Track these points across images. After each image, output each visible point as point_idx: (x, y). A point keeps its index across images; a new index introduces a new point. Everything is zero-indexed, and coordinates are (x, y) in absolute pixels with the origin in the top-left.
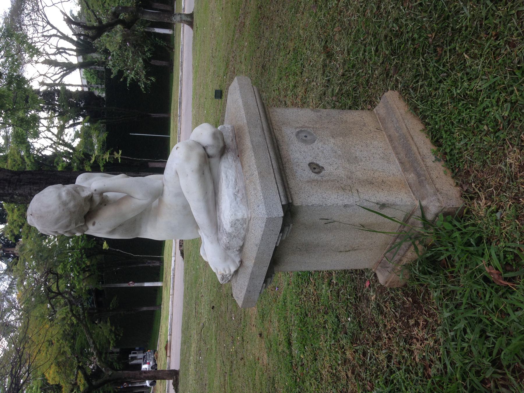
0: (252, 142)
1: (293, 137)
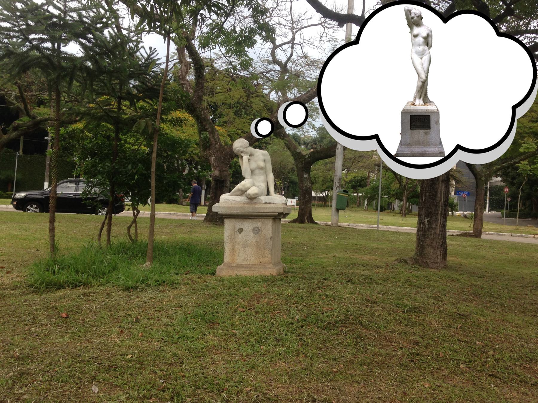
0: (245, 207)
1: (256, 226)
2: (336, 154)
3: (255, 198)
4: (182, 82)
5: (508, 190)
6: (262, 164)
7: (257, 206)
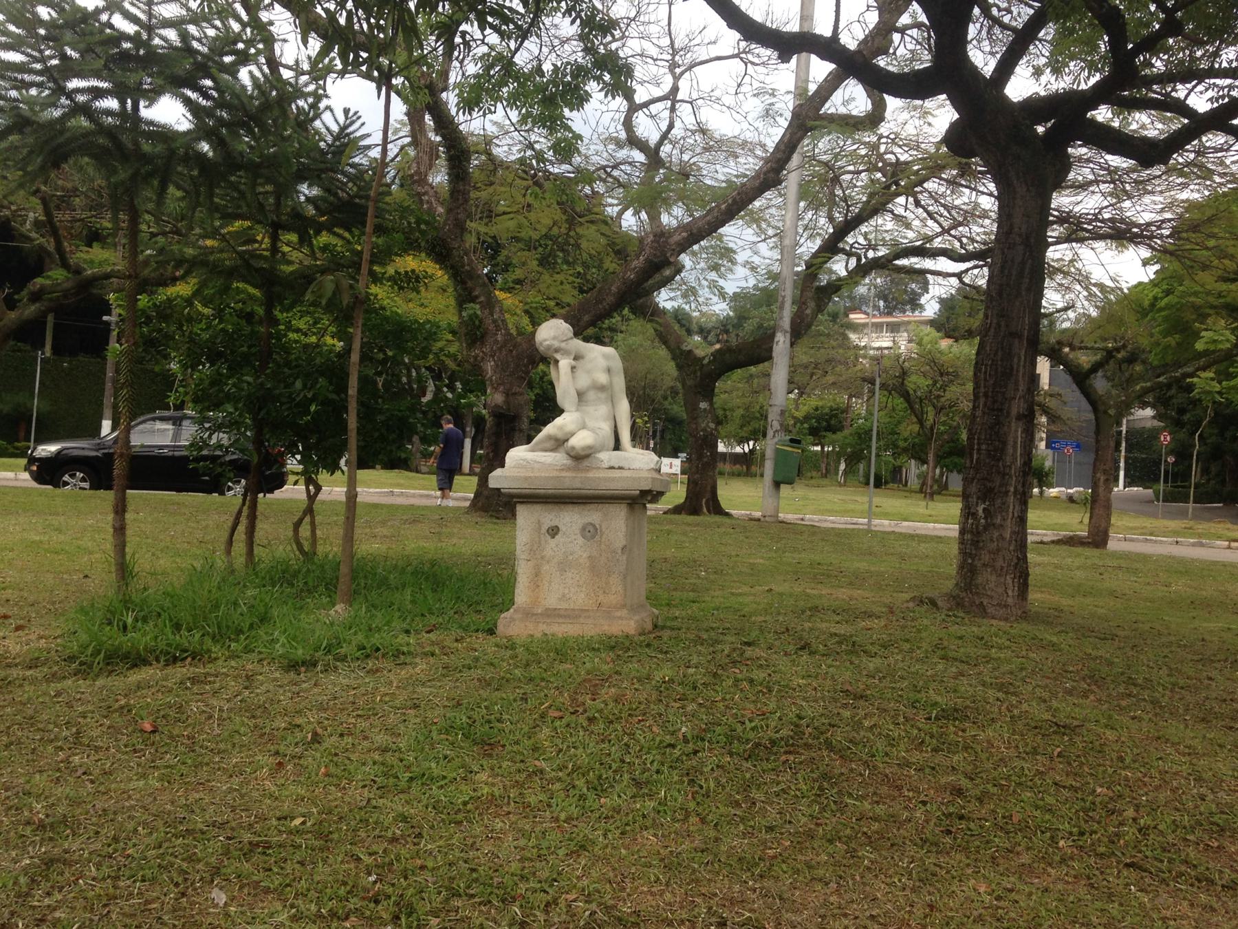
0: (565, 477)
1: (590, 520)
2: (774, 354)
3: (588, 456)
4: (419, 189)
5: (1168, 438)
6: (603, 378)
7: (590, 475)
